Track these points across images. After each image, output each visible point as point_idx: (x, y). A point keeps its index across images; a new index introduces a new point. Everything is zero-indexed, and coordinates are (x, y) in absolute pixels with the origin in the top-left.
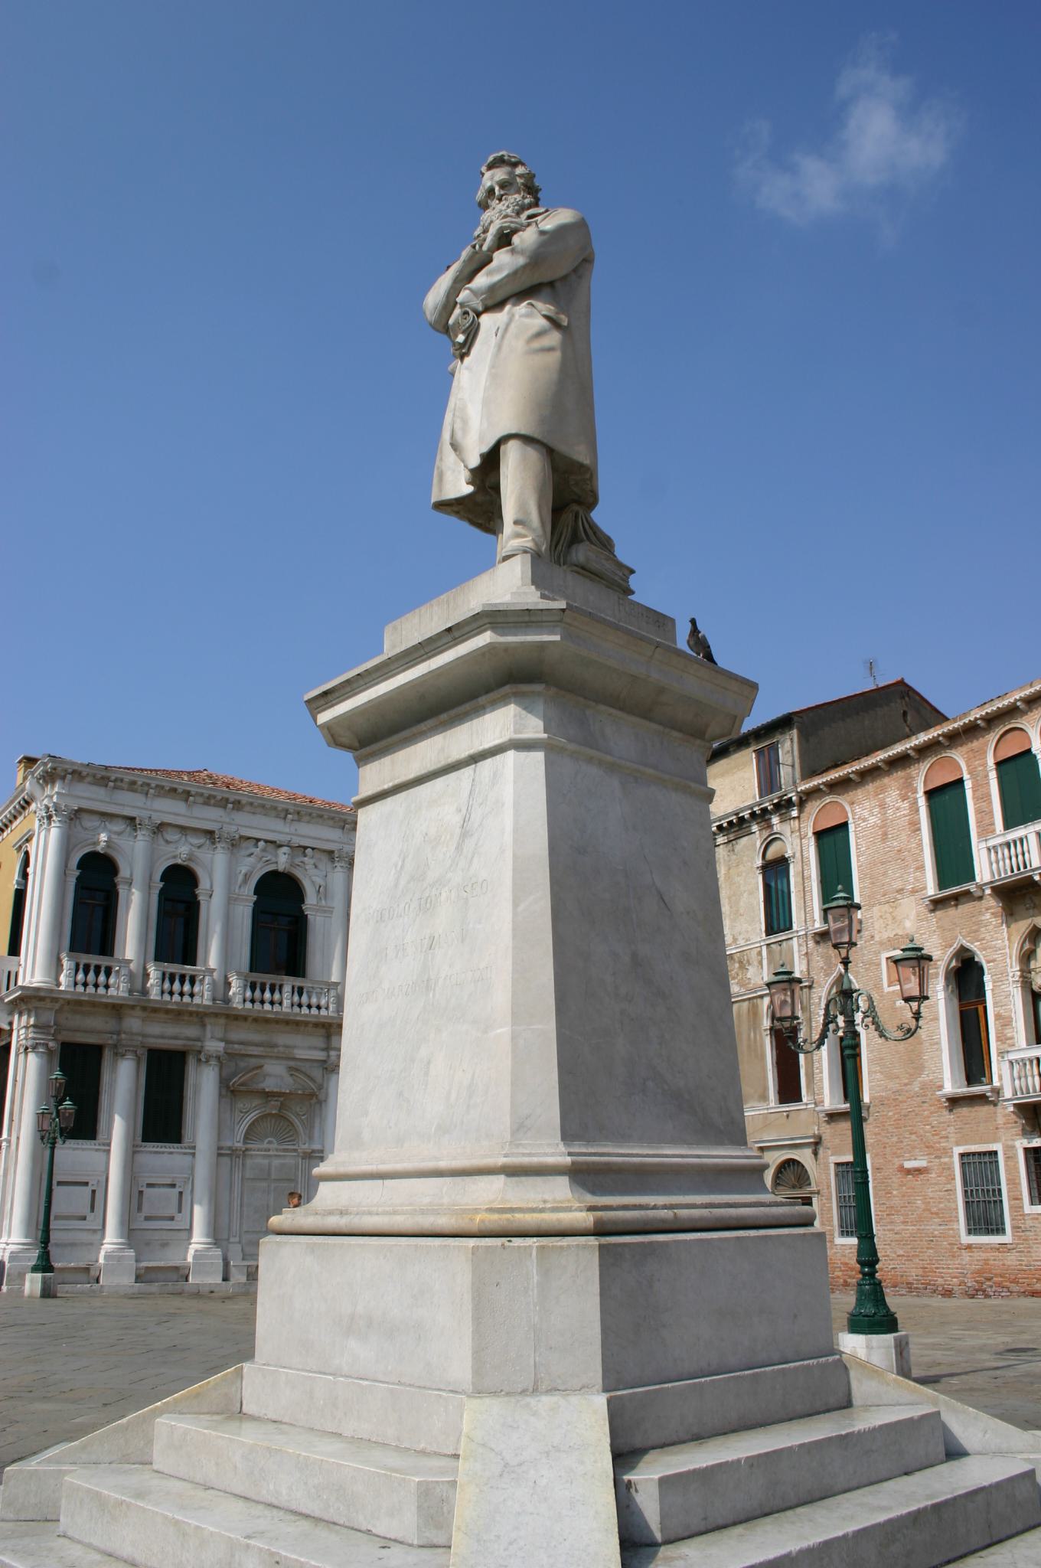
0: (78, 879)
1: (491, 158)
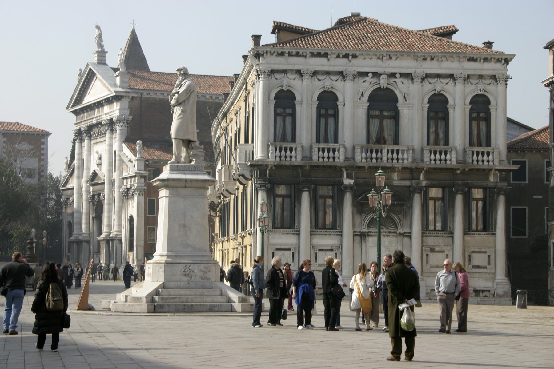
0: (275, 104)
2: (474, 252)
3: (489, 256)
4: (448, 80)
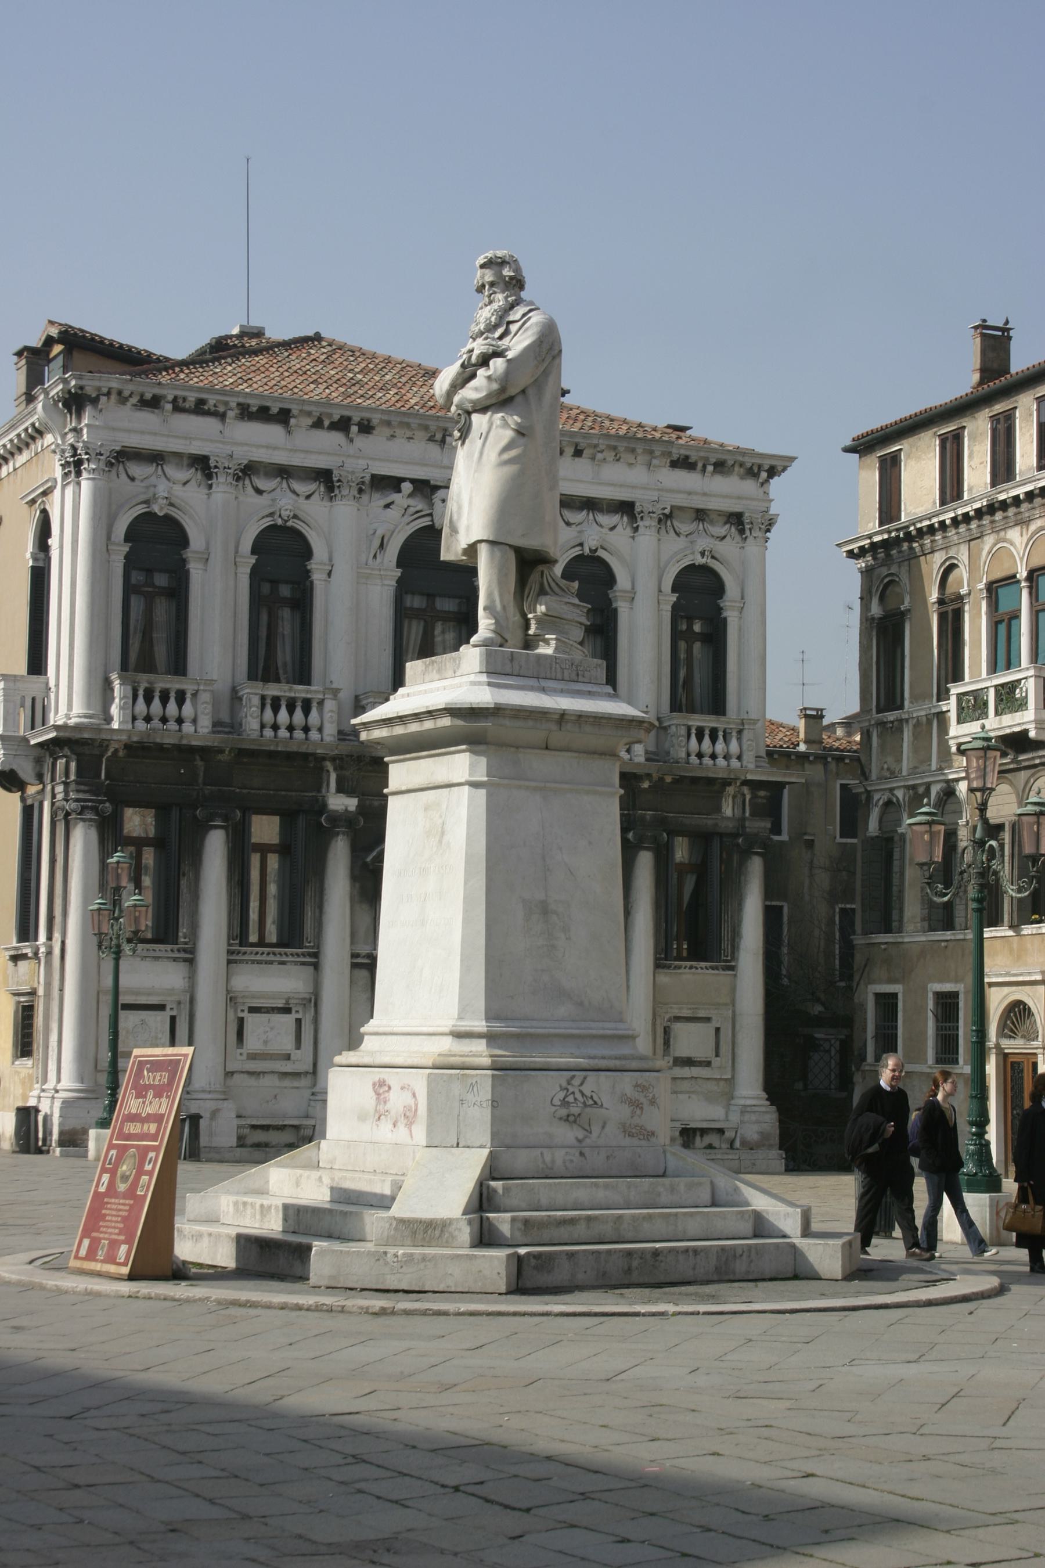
0: (127, 557)
1: (489, 254)
2: (678, 1019)
3: (718, 1030)
4: (615, 519)
